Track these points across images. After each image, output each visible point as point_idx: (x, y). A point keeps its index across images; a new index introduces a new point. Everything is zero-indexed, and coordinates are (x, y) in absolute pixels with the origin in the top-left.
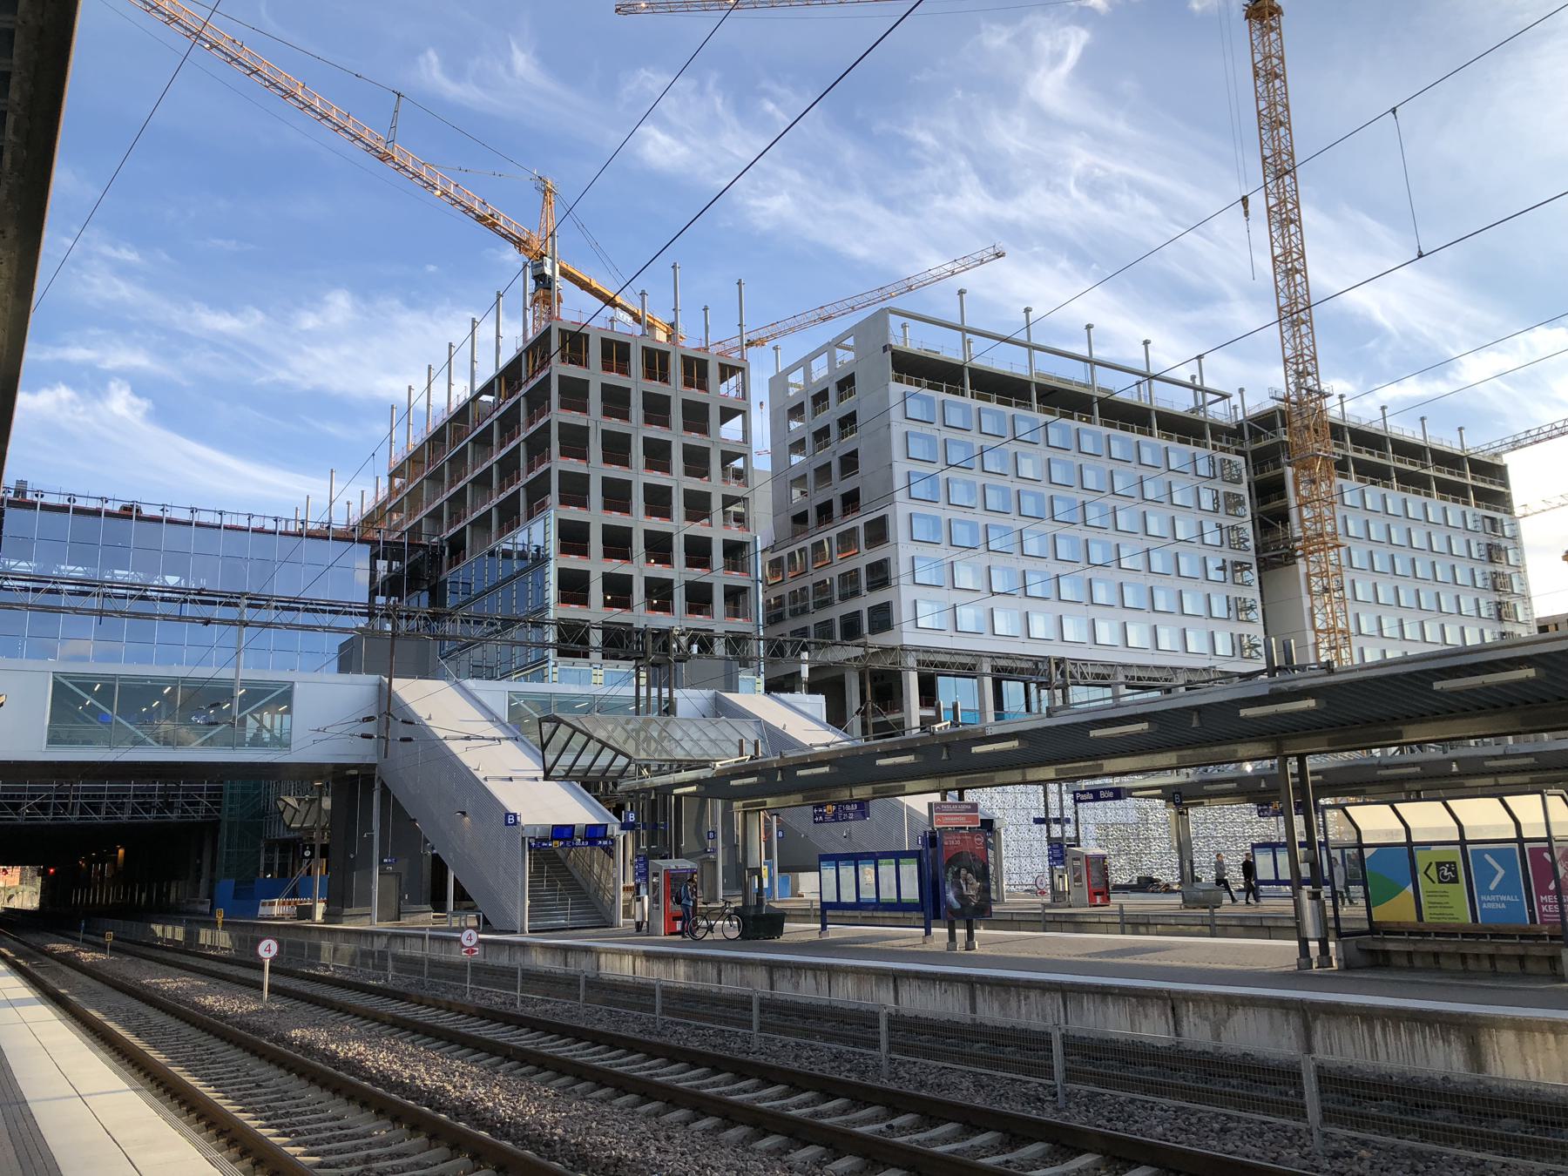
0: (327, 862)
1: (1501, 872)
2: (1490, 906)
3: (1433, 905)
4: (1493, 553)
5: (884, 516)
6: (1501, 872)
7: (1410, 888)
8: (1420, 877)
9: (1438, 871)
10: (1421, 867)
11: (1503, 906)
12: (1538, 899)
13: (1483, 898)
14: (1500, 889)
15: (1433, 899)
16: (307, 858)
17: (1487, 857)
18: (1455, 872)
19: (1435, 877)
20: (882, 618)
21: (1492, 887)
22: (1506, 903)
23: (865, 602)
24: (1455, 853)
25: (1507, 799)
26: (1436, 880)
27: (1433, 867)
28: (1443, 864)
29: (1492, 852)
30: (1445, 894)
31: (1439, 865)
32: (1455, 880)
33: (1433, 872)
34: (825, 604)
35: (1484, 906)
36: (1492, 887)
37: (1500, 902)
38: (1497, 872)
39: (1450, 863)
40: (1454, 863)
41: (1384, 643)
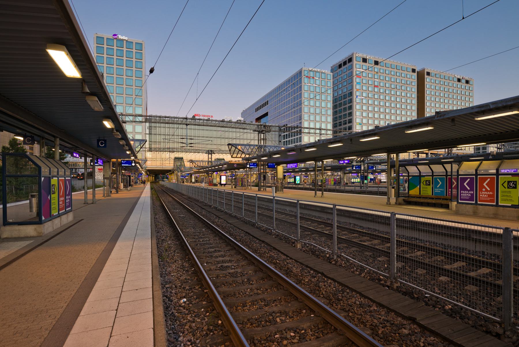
0: (398, 214)
1: (465, 184)
2: (436, 191)
3: (423, 191)
4: (340, 154)
5: (351, 105)
6: (465, 184)
7: (419, 187)
8: (422, 184)
9: (426, 182)
10: (422, 182)
11: (470, 195)
12: (460, 192)
13: (462, 192)
14: (439, 188)
15: (424, 189)
16: (62, 197)
17: (438, 179)
18: (430, 183)
19: (506, 186)
20: (350, 128)
21: (438, 187)
22: (441, 191)
23: (348, 125)
24: (430, 178)
25: (431, 166)
26: (425, 185)
27: (506, 183)
28: (427, 181)
29: (439, 178)
30: (510, 192)
31: (426, 181)
32: (429, 185)
33: (424, 183)
34: (346, 124)
35: (462, 195)
36: (438, 187)
37: (439, 190)
38: (467, 184)
39: (514, 182)
40: (430, 181)
41: (462, 106)
